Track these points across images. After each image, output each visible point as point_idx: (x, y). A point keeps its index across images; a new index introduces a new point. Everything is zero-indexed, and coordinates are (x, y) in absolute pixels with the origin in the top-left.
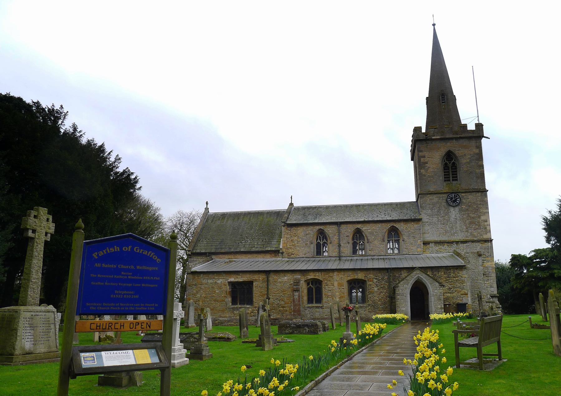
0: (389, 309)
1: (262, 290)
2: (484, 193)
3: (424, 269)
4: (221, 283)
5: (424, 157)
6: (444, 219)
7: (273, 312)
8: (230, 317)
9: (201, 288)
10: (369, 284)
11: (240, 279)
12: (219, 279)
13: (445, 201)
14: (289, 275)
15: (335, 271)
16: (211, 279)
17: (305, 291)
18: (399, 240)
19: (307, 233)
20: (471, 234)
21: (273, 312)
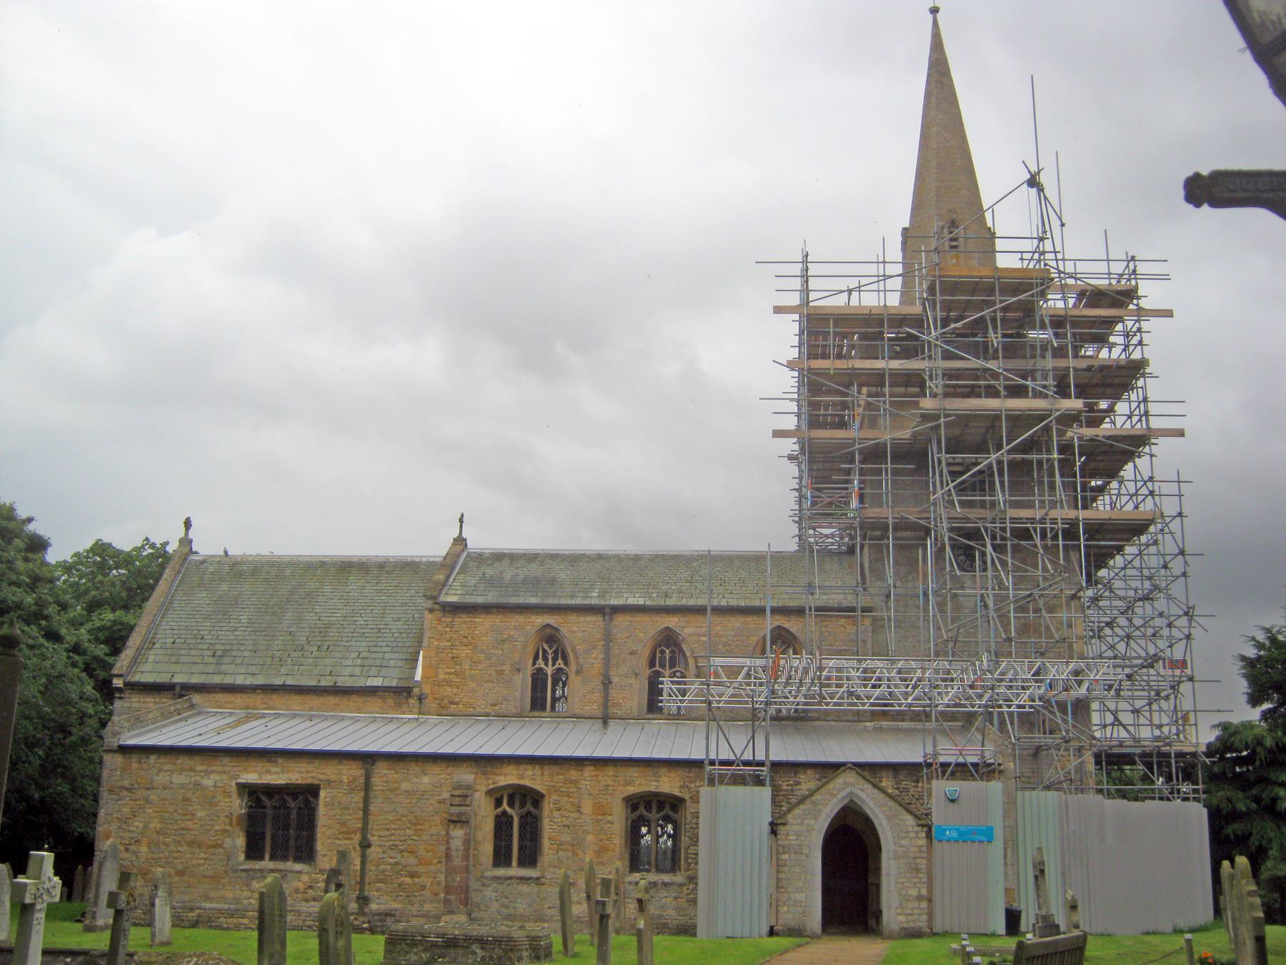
3: (870, 770)
9: (147, 801)
11: (278, 776)
12: (207, 773)
15: (587, 765)
16: (182, 770)
17: (489, 827)
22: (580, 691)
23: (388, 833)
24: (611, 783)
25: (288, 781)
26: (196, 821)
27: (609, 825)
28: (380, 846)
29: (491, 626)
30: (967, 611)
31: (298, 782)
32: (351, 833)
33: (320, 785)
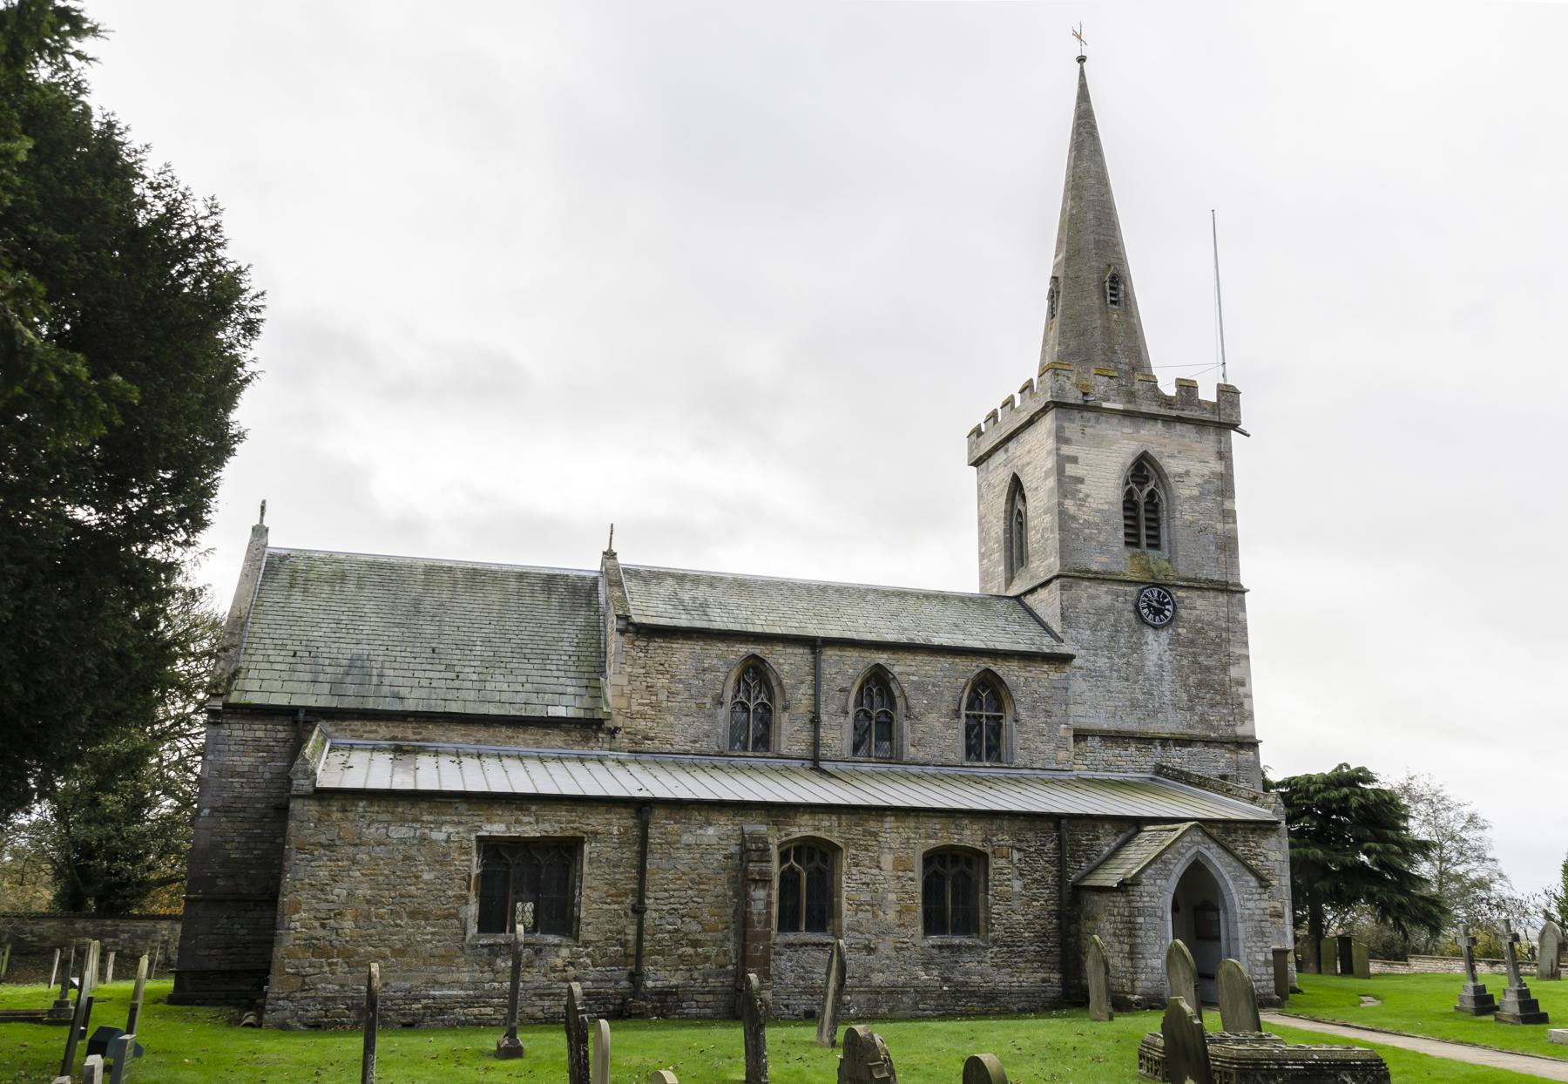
0: (1057, 959)
1: (615, 873)
2: (1238, 596)
4: (446, 842)
5: (1074, 460)
6: (1128, 663)
7: (656, 963)
8: (476, 984)
9: (354, 862)
10: (995, 866)
11: (530, 827)
12: (439, 825)
13: (1130, 607)
14: (723, 820)
15: (887, 816)
16: (403, 821)
18: (1001, 717)
19: (706, 665)
20: (1203, 720)
21: (656, 963)
22: (790, 734)
23: (667, 894)
24: (913, 836)
25: (544, 834)
26: (421, 885)
27: (910, 882)
28: (656, 910)
29: (691, 654)
30: (1151, 663)
31: (556, 835)
32: (621, 896)
33: (583, 838)
